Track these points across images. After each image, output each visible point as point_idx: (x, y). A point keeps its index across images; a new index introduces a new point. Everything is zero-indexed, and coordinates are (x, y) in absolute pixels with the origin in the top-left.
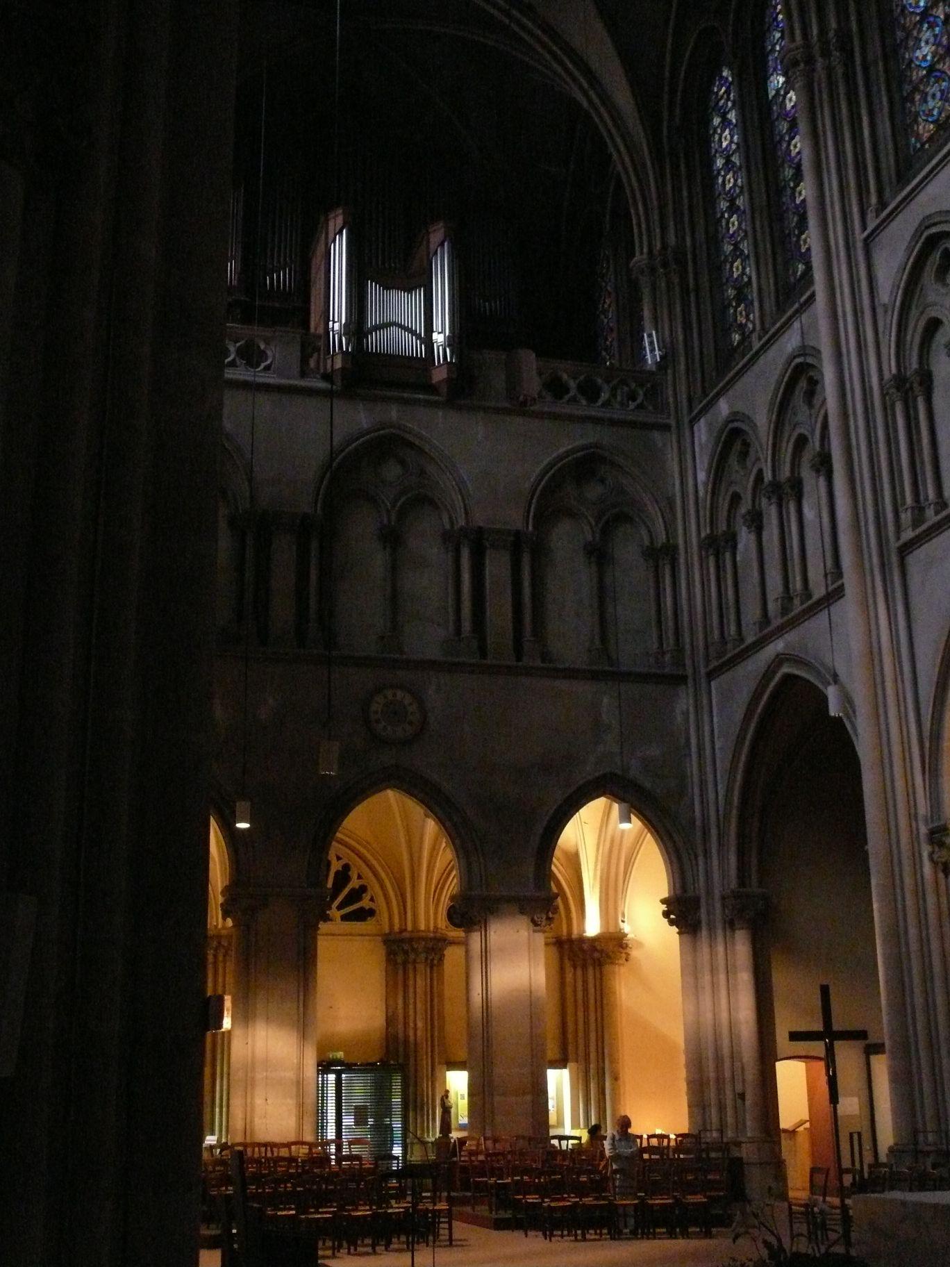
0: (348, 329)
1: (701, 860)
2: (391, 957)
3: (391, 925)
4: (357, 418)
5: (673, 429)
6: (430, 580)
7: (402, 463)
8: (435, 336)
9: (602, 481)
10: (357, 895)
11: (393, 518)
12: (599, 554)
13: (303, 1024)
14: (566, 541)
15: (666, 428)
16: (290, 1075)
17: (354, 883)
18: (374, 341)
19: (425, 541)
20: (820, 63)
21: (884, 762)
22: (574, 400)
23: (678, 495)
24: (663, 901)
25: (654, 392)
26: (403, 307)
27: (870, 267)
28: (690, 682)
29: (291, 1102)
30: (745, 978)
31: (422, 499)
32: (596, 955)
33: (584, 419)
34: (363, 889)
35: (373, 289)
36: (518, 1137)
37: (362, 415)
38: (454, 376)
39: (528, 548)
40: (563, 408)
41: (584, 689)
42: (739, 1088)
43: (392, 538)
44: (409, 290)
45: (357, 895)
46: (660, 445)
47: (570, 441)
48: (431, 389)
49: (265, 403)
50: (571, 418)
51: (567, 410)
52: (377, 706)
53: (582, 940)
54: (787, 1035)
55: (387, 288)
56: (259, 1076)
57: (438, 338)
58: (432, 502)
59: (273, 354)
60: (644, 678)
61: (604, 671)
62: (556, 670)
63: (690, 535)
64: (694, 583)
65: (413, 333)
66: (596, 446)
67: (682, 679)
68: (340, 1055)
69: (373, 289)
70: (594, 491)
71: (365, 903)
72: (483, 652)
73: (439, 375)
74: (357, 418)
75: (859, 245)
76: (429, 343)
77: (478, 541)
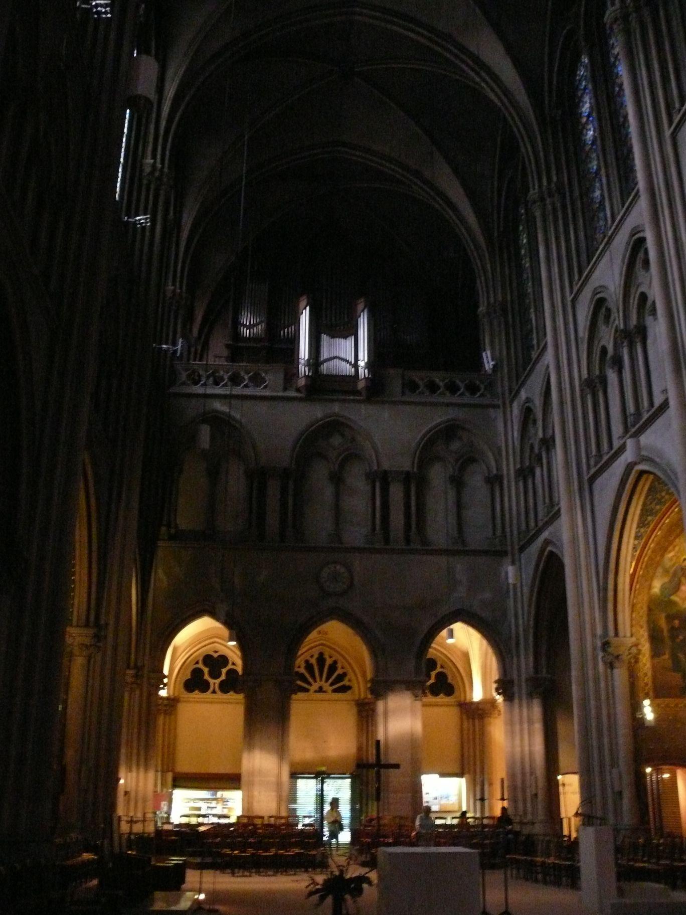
0: (308, 364)
1: (515, 660)
2: (360, 713)
3: (360, 695)
4: (317, 412)
6: (359, 501)
7: (343, 435)
8: (359, 363)
9: (460, 439)
10: (341, 677)
12: (458, 482)
13: (281, 751)
14: (438, 475)
15: (495, 407)
16: (273, 779)
17: (339, 671)
19: (356, 478)
20: (548, 201)
21: (580, 605)
22: (443, 394)
23: (503, 445)
24: (496, 682)
25: (490, 386)
26: (343, 348)
27: (574, 316)
29: (274, 794)
30: (538, 727)
31: (351, 456)
32: (480, 712)
33: (448, 405)
34: (345, 674)
35: (325, 338)
36: (271, 817)
37: (386, 415)
39: (415, 481)
40: (435, 399)
41: (443, 560)
42: (617, 789)
44: (345, 337)
45: (341, 677)
46: (493, 417)
47: (439, 417)
48: (356, 392)
49: (262, 408)
50: (435, 405)
51: (441, 400)
52: (340, 569)
53: (472, 703)
54: (401, 766)
55: (333, 337)
56: (257, 779)
57: (362, 364)
59: (269, 378)
60: (486, 553)
61: (460, 548)
62: (436, 551)
63: (509, 468)
64: (512, 495)
65: (347, 362)
66: (453, 420)
67: (504, 553)
68: (324, 769)
69: (325, 338)
70: (455, 446)
71: (346, 682)
72: (387, 540)
73: (361, 385)
74: (317, 412)
75: (569, 304)
76: (356, 366)
77: (381, 479)
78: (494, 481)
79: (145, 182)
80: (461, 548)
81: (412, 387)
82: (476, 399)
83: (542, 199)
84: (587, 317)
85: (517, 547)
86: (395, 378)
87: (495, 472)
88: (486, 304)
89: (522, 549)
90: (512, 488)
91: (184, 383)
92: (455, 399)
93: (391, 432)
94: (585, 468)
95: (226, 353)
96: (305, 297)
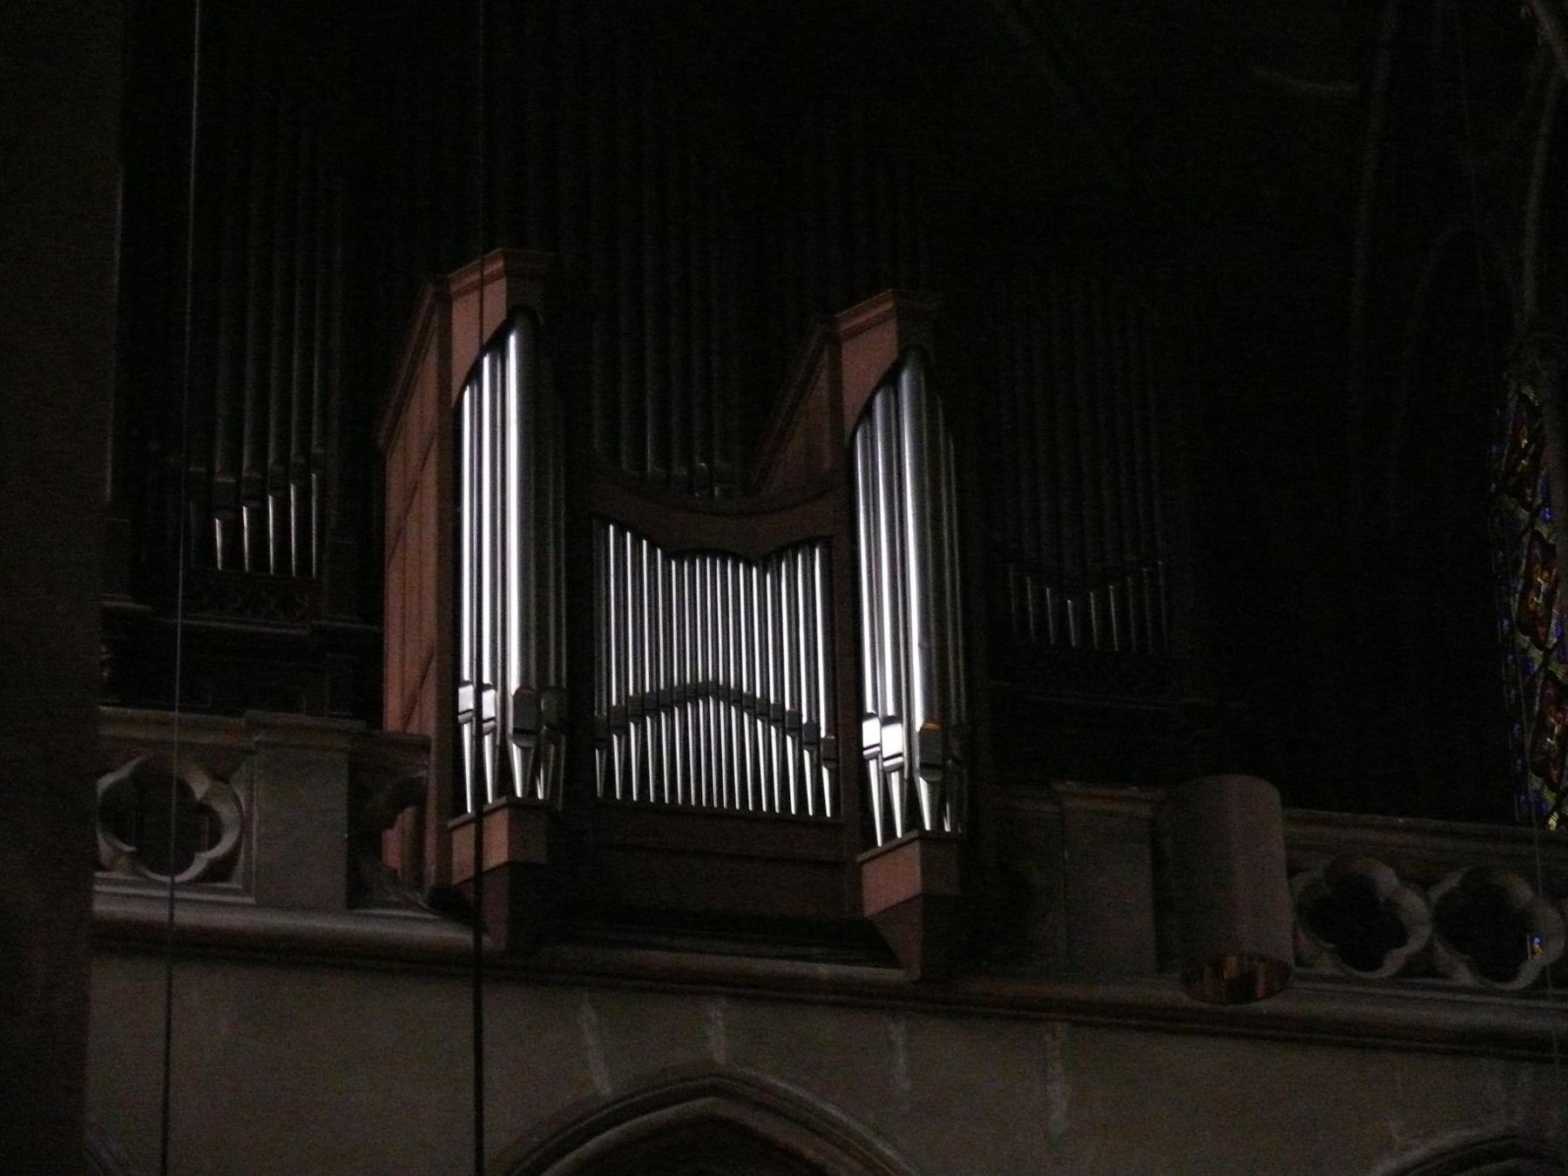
69: (626, 561)
76: (848, 758)
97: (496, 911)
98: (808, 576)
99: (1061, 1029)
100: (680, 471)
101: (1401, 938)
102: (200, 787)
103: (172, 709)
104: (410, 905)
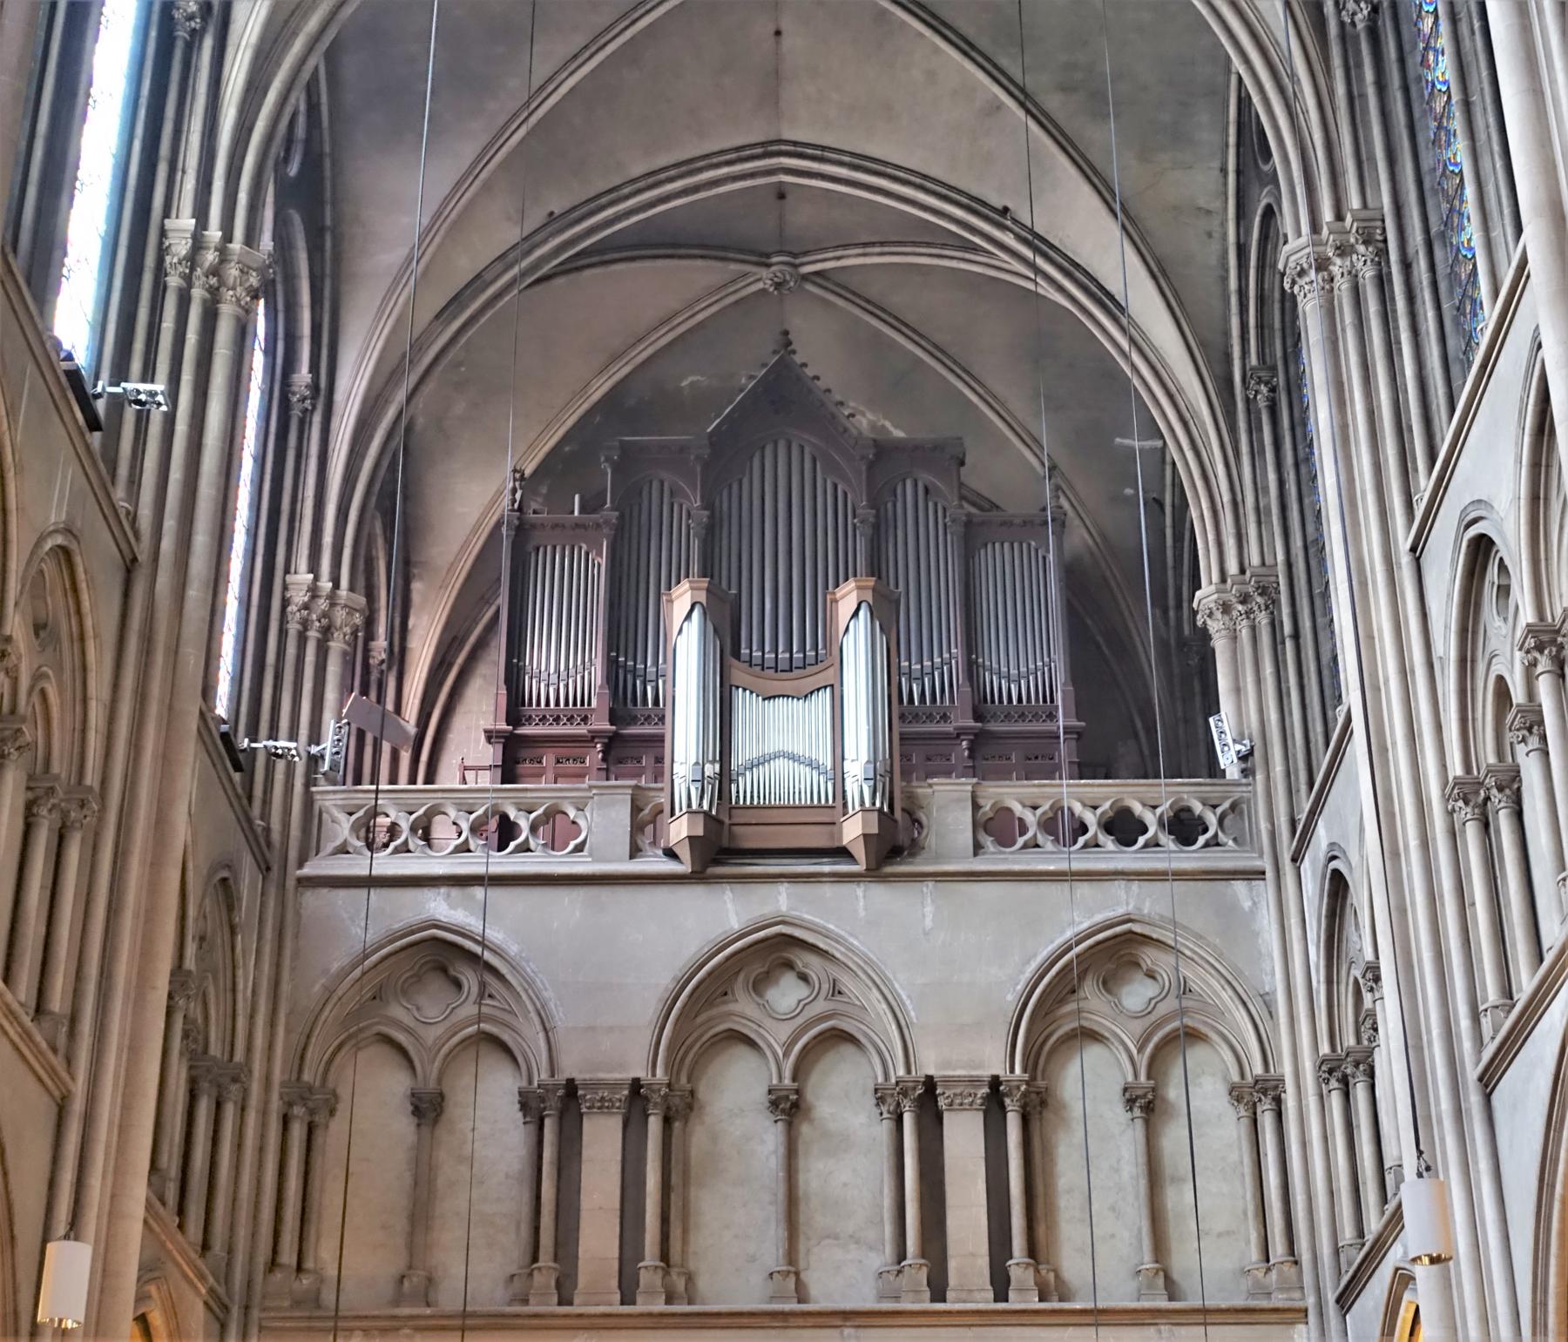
4: (728, 912)
5: (1270, 875)
9: (1151, 975)
11: (787, 1073)
12: (1147, 1105)
18: (744, 788)
19: (845, 1102)
28: (1312, 1317)
37: (929, 909)
38: (700, 832)
39: (1021, 1107)
43: (789, 1107)
46: (1247, 904)
47: (1079, 914)
58: (850, 1038)
63: (1298, 1058)
65: (810, 764)
69: (746, 706)
70: (1136, 994)
72: (938, 1290)
74: (728, 912)
76: (838, 777)
78: (1259, 1095)
79: (174, 281)
80: (1164, 1304)
81: (996, 827)
82: (1191, 858)
83: (1322, 264)
84: (1450, 596)
85: (1331, 1297)
86: (949, 805)
87: (1258, 1069)
88: (1215, 577)
89: (1346, 1300)
90: (1309, 1108)
91: (343, 850)
92: (1129, 859)
93: (941, 963)
94: (1467, 1045)
95: (490, 754)
96: (685, 585)
97: (685, 853)
98: (824, 699)
99: (931, 884)
100: (630, 663)
101: (1206, 830)
102: (572, 813)
103: (1051, 773)
104: (656, 856)
